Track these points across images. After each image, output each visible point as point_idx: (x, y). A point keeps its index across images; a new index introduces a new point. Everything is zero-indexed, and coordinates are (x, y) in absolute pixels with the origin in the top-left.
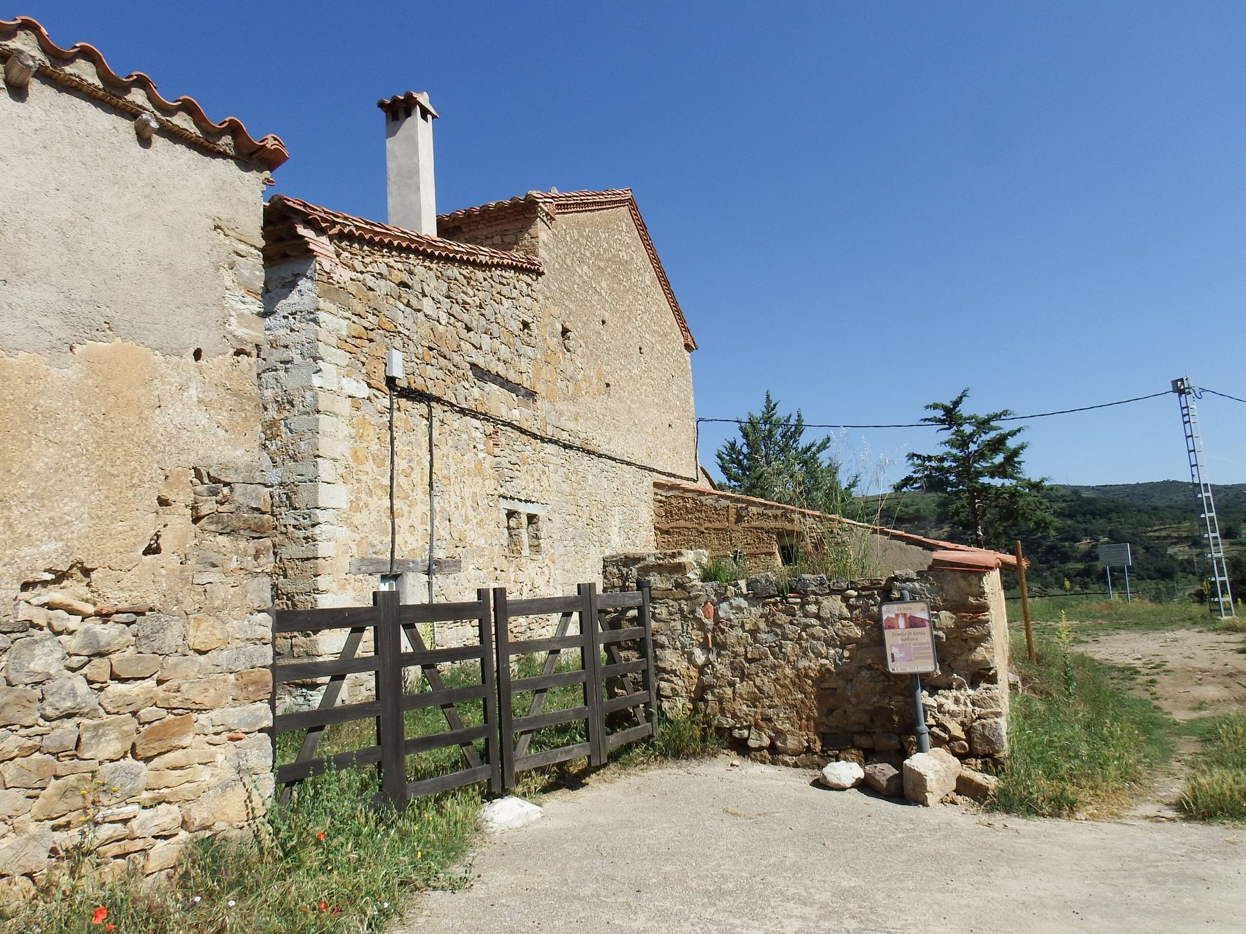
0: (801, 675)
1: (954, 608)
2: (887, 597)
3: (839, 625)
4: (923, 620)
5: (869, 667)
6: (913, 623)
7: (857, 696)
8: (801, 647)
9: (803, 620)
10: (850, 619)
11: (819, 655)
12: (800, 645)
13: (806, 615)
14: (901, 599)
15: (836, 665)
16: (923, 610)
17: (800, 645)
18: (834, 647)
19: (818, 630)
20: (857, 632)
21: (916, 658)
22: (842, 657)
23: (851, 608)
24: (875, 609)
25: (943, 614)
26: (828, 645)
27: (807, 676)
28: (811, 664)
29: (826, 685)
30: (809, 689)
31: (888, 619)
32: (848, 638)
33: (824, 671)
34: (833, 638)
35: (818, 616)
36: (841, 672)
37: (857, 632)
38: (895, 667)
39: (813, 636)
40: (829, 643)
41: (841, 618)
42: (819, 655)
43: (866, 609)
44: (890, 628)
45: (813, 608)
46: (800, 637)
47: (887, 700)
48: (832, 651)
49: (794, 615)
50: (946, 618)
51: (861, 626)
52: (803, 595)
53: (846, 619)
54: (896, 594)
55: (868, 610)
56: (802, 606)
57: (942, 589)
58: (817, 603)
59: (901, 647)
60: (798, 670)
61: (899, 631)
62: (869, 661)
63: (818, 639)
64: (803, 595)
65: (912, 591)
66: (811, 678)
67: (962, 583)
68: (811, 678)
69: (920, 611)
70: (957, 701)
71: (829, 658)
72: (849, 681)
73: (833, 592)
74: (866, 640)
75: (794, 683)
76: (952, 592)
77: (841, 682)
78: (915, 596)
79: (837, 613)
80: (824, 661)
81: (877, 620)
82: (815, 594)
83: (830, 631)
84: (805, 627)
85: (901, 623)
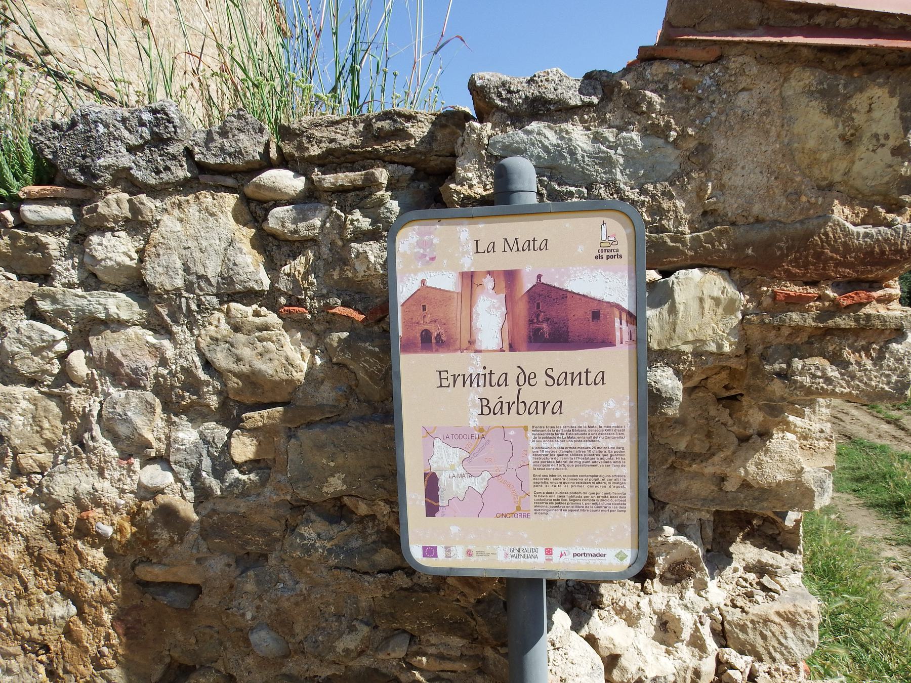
0: (66, 528)
1: (748, 257)
2: (429, 184)
3: (218, 324)
4: (598, 312)
5: (337, 511)
6: (551, 321)
7: (281, 623)
8: (67, 414)
9: (79, 300)
10: (269, 299)
11: (134, 448)
12: (63, 401)
13: (92, 280)
14: (501, 198)
15: (203, 494)
16: (606, 253)
17: (63, 401)
18: (197, 413)
19: (134, 345)
20: (290, 356)
21: (545, 505)
22: (223, 463)
23: (273, 247)
24: (373, 251)
25: (694, 285)
26: (171, 407)
27: (83, 530)
28: (106, 487)
29: (154, 573)
30: (94, 587)
31: (425, 297)
32: (252, 379)
33: (155, 522)
34: (193, 384)
35: (137, 286)
36: (220, 524)
37: (290, 356)
38: (442, 543)
39: (112, 369)
40: (177, 398)
41: (232, 292)
42: (134, 448)
43: (335, 254)
44: (429, 341)
45: (115, 249)
46: (66, 376)
47: (398, 650)
48: (188, 434)
49: (46, 278)
50: (705, 307)
51: (313, 328)
52: (82, 190)
53: (248, 296)
54: (473, 180)
55: (341, 258)
56: (79, 238)
57: (700, 155)
58: (136, 224)
59: (474, 442)
60: (53, 505)
61: (473, 364)
62: (336, 484)
63: (134, 382)
64: (82, 190)
65: (553, 170)
66: (99, 540)
67: (814, 124)
68: (99, 540)
69: (589, 260)
70: (666, 629)
71: (174, 462)
72: (250, 561)
73: (204, 176)
74: (327, 394)
75: (38, 561)
76: (747, 174)
77: (217, 565)
78: (566, 186)
79: (213, 269)
80: (153, 475)
81: (373, 302)
82: (134, 186)
83: (182, 350)
84: (86, 329)
85: (489, 318)
